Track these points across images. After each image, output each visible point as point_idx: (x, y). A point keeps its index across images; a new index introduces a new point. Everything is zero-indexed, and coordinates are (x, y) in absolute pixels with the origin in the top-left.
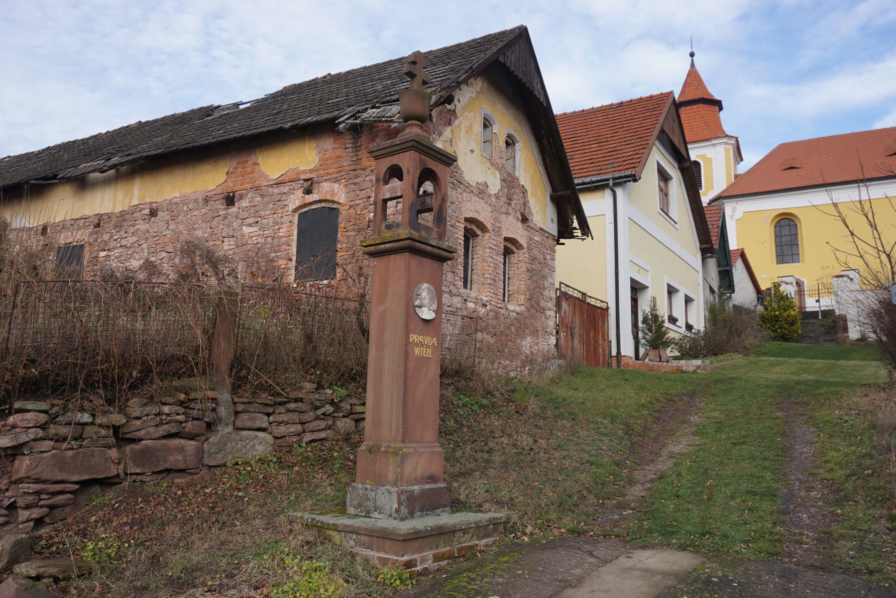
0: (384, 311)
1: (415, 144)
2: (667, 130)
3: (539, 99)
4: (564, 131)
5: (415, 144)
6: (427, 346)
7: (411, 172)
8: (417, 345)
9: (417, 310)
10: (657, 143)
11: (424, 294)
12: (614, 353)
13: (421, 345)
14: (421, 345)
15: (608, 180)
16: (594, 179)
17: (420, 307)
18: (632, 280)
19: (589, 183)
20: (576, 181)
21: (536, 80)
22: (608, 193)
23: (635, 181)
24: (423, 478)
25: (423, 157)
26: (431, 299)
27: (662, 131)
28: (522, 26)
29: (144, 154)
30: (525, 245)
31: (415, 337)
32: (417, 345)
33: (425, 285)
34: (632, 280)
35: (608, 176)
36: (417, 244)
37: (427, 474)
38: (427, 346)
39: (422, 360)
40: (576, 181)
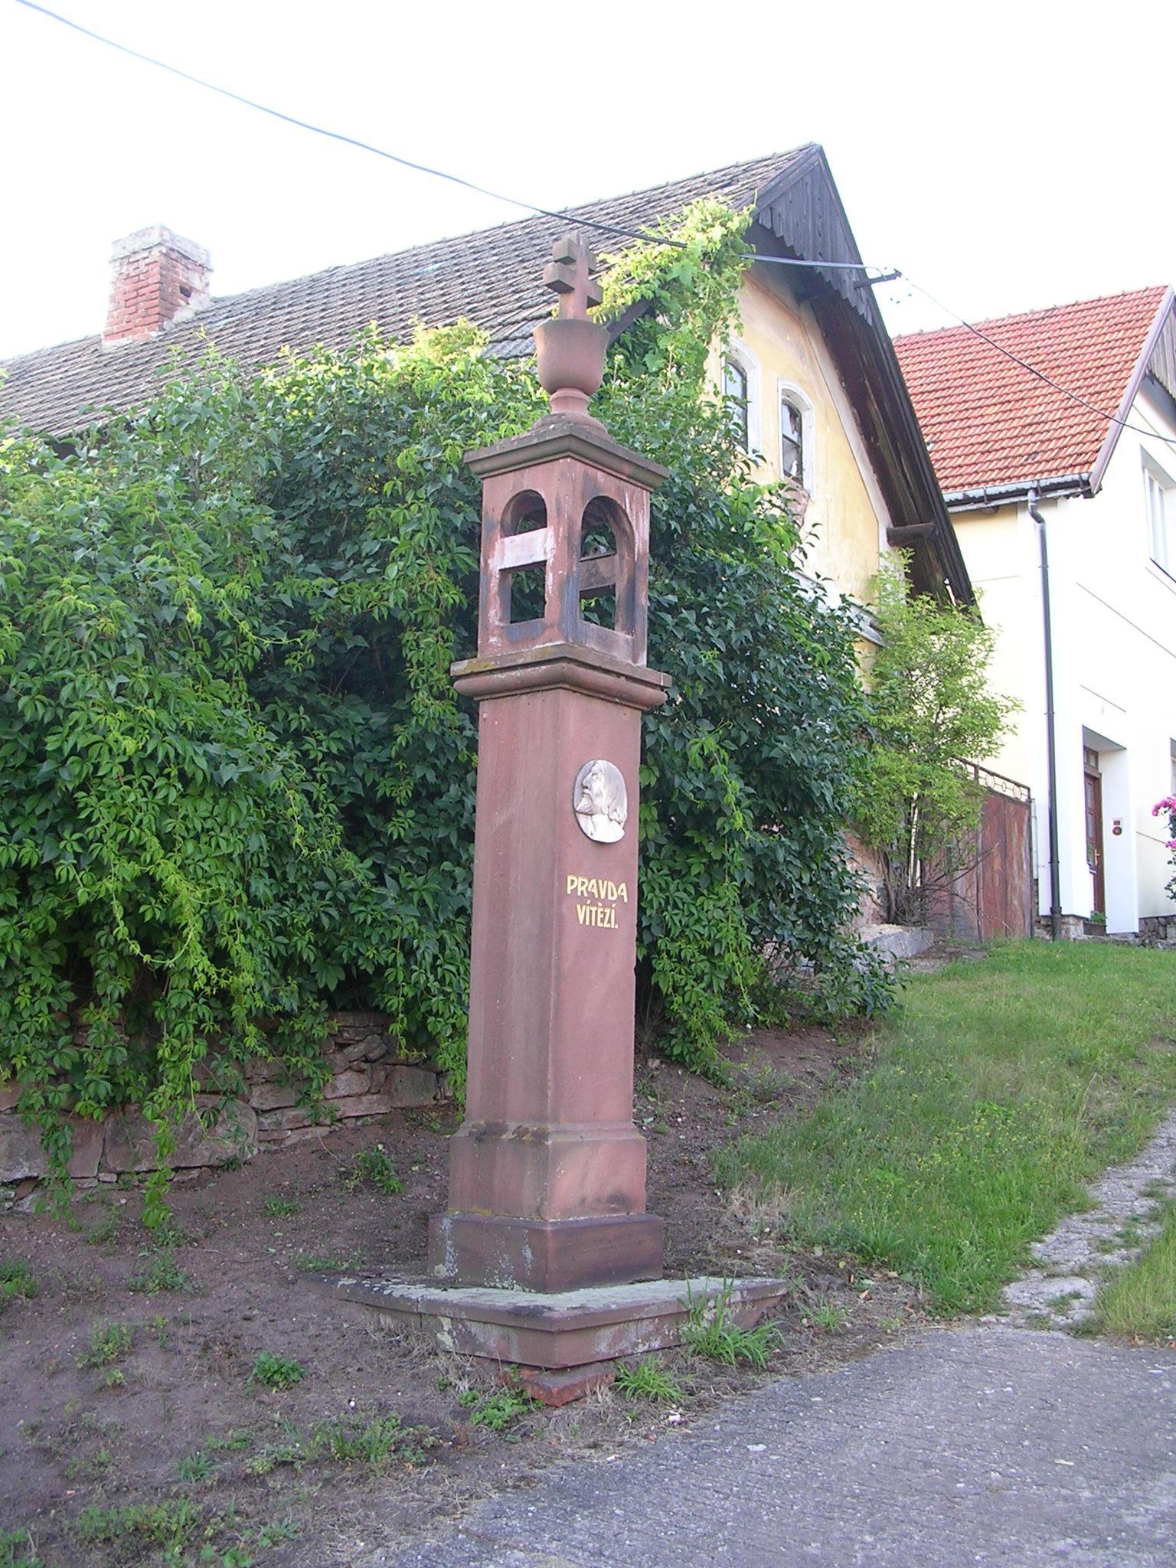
0: (508, 824)
1: (574, 445)
2: (1160, 373)
3: (855, 309)
4: (914, 374)
5: (574, 445)
6: (606, 903)
7: (566, 507)
8: (582, 900)
9: (582, 819)
10: (1140, 402)
11: (598, 785)
12: (1044, 908)
13: (594, 900)
14: (594, 900)
15: (1024, 492)
16: (992, 490)
17: (590, 814)
18: (1087, 732)
19: (980, 500)
20: (947, 496)
21: (840, 232)
22: (1024, 519)
23: (1088, 494)
24: (599, 1200)
25: (591, 471)
26: (614, 797)
27: (1150, 377)
28: (811, 145)
29: (1044, 1333)
30: (974, 1059)
31: (578, 881)
32: (582, 900)
33: (601, 764)
34: (1087, 732)
35: (1026, 484)
36: (581, 671)
37: (609, 1190)
38: (606, 903)
39: (593, 932)
40: (947, 496)
